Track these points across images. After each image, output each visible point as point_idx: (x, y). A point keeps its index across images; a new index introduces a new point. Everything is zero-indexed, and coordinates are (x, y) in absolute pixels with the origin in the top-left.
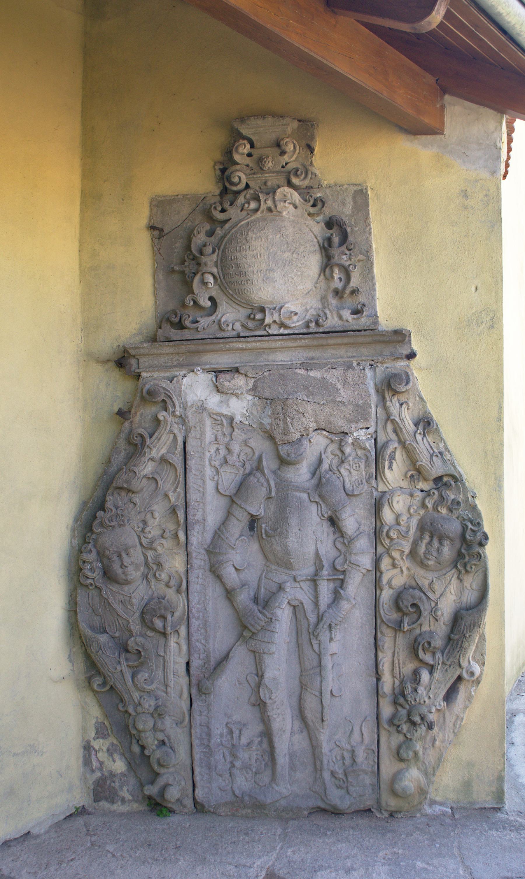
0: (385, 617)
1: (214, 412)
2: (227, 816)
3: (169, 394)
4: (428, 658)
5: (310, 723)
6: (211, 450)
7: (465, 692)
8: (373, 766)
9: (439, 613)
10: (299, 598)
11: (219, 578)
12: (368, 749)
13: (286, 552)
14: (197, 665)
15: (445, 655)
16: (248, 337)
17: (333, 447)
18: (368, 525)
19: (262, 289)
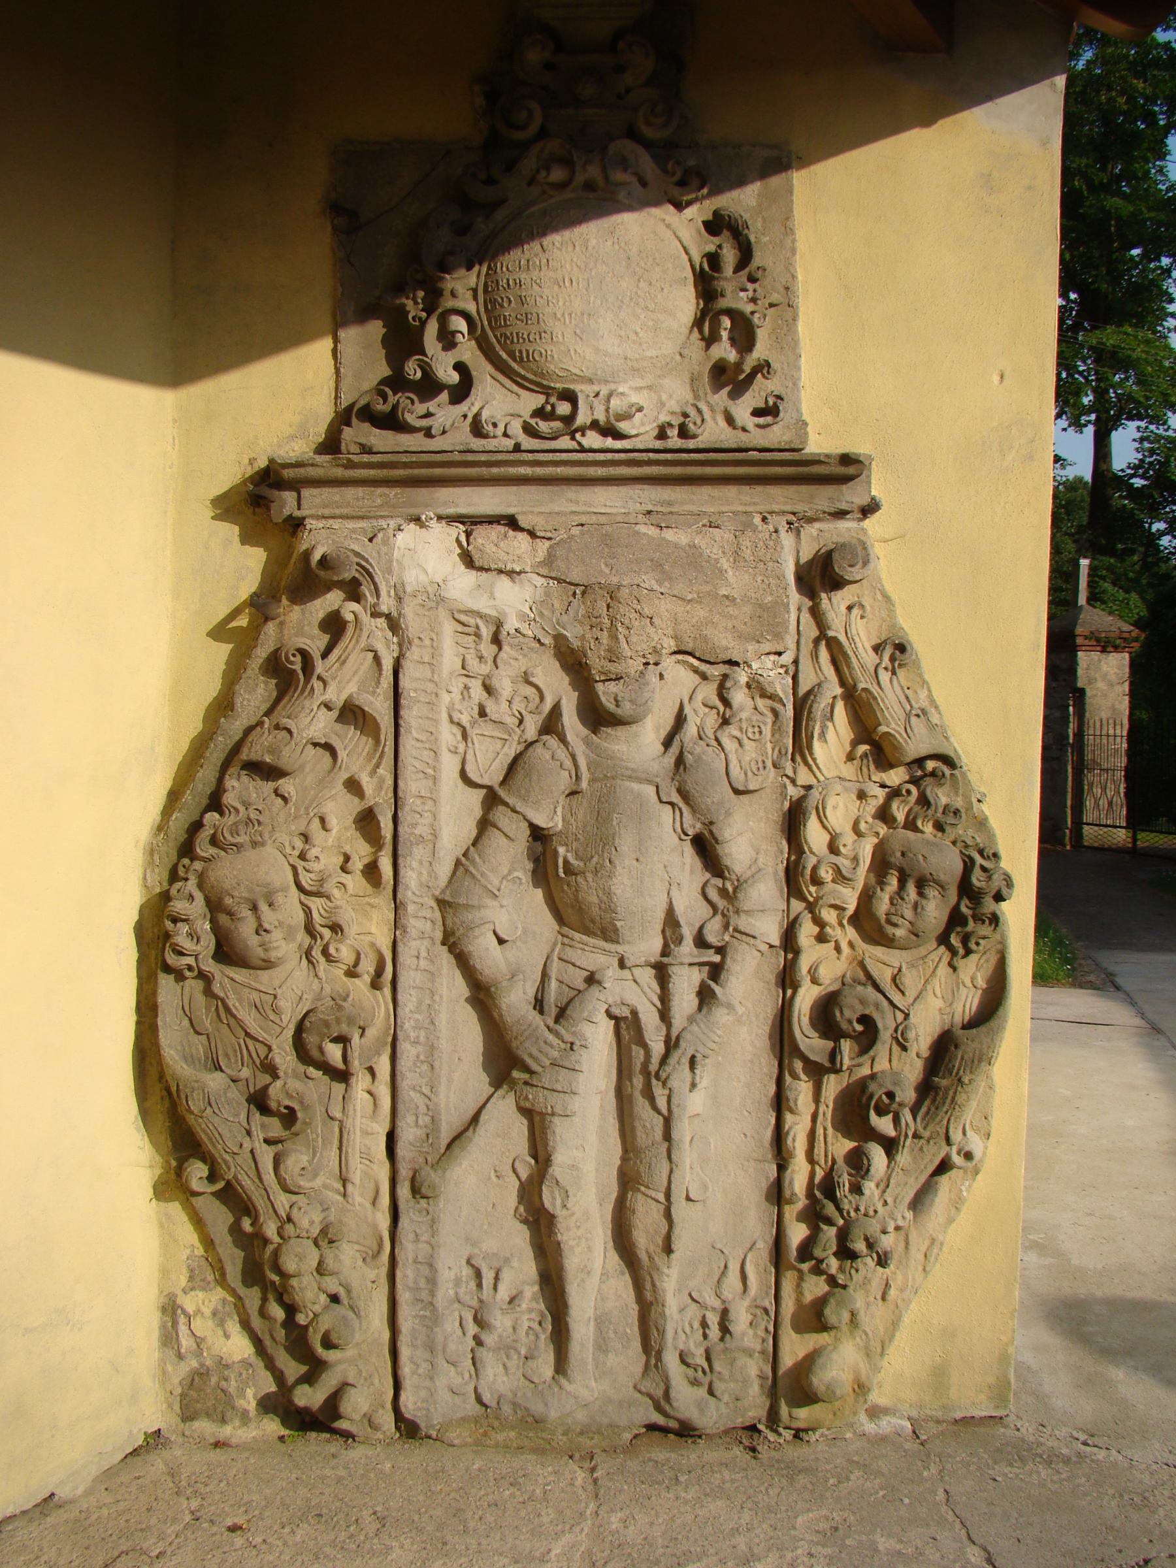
0: (803, 1041)
1: (462, 608)
2: (466, 1445)
3: (368, 567)
4: (884, 1125)
5: (643, 1256)
6: (452, 689)
7: (950, 1191)
8: (763, 1341)
9: (911, 1035)
10: (630, 1002)
12: (756, 1307)
13: (609, 907)
14: (411, 1138)
15: (918, 1119)
16: (538, 452)
17: (709, 691)
19: (572, 352)
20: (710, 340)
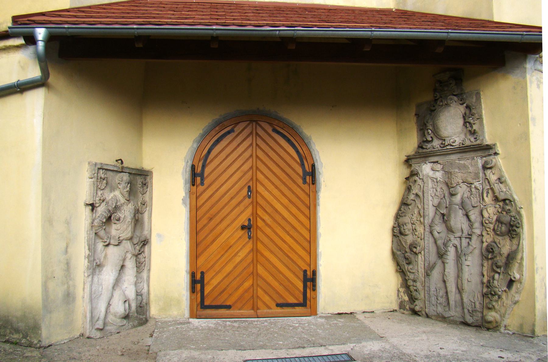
11: (432, 235)
17: (468, 189)
18: (479, 219)
20: (466, 127)
